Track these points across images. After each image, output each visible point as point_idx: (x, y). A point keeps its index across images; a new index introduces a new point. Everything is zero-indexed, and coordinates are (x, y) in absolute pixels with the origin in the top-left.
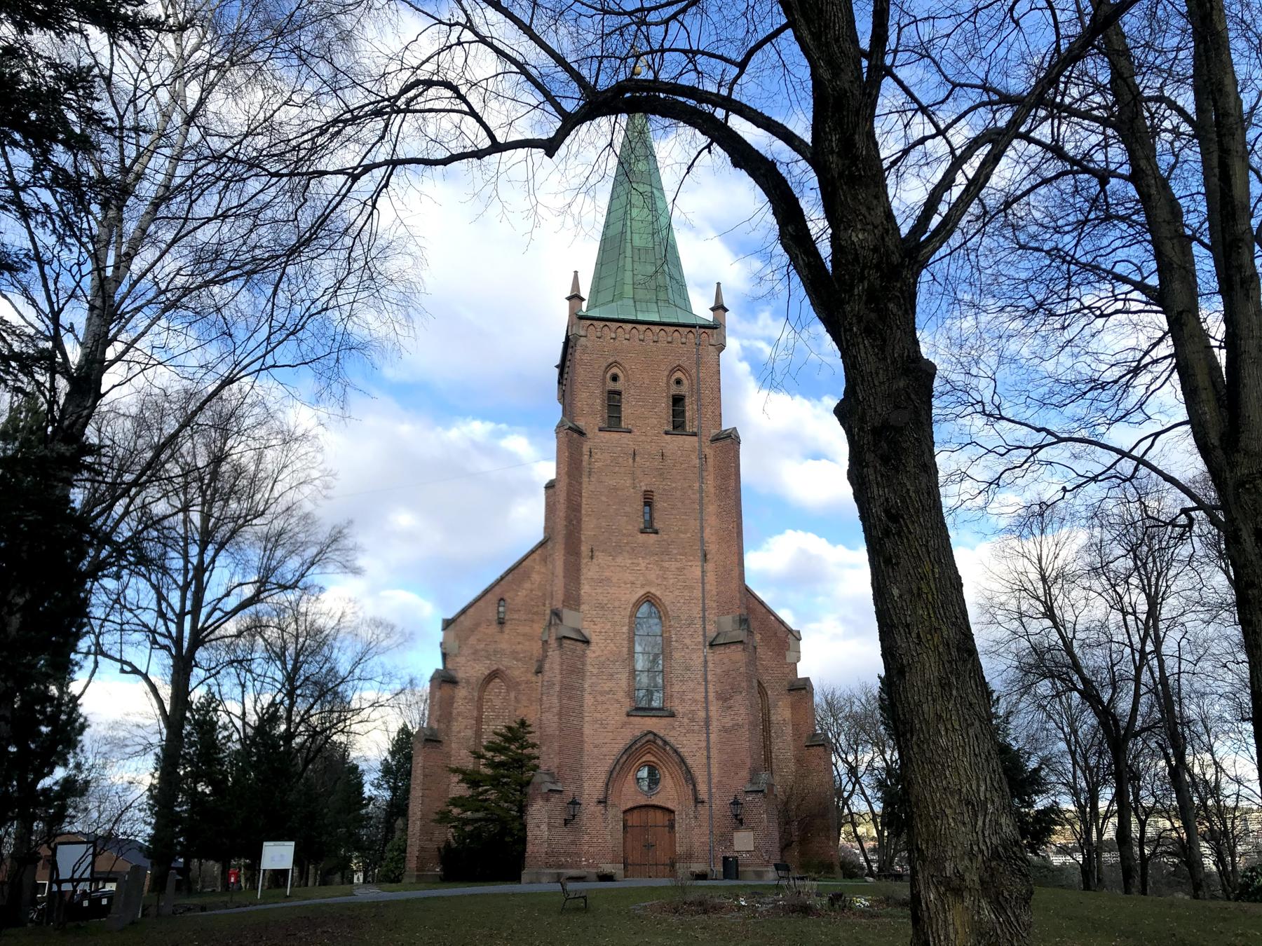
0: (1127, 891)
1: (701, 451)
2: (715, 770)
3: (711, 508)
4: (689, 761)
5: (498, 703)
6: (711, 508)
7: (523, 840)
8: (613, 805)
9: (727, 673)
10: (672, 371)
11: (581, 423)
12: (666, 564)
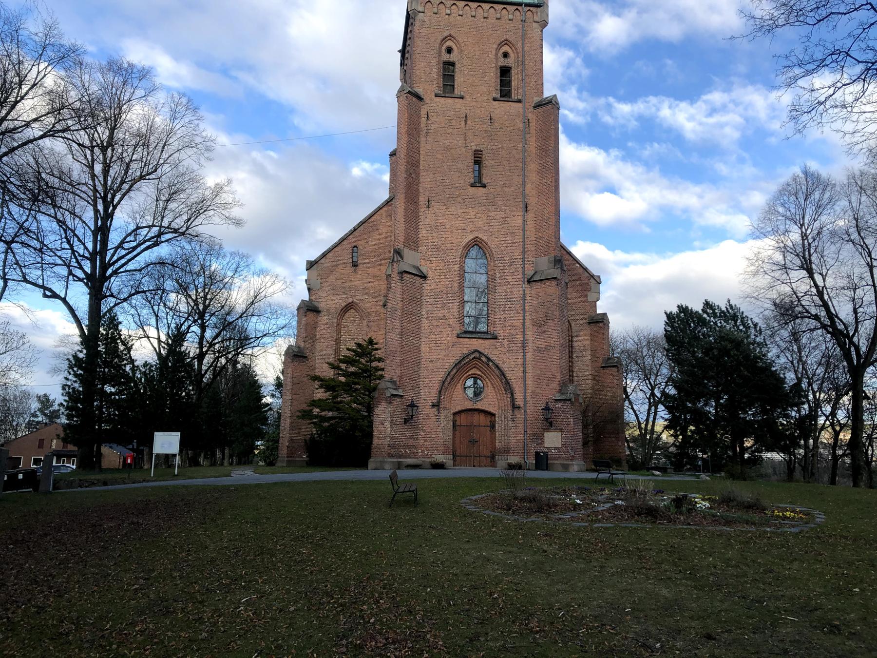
0: (856, 485)
1: (524, 116)
2: (529, 381)
3: (532, 166)
4: (508, 375)
5: (353, 328)
6: (532, 166)
7: (369, 435)
8: (445, 408)
9: (542, 304)
10: (500, 45)
11: (419, 90)
12: (492, 214)
